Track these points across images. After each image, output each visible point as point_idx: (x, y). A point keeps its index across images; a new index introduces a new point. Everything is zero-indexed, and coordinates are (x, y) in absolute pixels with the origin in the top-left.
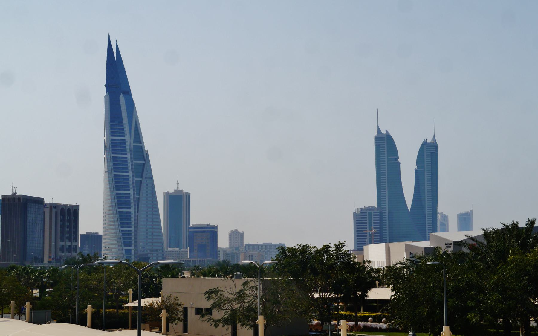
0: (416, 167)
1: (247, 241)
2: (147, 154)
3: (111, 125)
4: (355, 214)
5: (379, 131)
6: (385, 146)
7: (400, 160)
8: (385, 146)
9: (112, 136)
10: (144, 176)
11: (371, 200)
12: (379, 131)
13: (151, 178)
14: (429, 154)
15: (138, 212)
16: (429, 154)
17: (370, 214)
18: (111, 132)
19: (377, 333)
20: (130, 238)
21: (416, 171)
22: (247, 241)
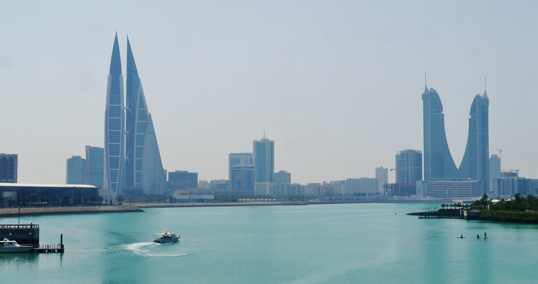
0: (470, 117)
1: (293, 181)
2: (150, 116)
3: (111, 96)
4: (397, 156)
5: (426, 89)
6: (432, 103)
7: (345, 179)
8: (432, 103)
9: (111, 104)
10: (147, 132)
11: (417, 143)
12: (426, 89)
13: (153, 133)
14: (480, 109)
15: (364, 195)
16: (480, 109)
17: (407, 155)
18: (111, 101)
19: (121, 85)
20: (117, 176)
21: (470, 120)
22: (293, 181)
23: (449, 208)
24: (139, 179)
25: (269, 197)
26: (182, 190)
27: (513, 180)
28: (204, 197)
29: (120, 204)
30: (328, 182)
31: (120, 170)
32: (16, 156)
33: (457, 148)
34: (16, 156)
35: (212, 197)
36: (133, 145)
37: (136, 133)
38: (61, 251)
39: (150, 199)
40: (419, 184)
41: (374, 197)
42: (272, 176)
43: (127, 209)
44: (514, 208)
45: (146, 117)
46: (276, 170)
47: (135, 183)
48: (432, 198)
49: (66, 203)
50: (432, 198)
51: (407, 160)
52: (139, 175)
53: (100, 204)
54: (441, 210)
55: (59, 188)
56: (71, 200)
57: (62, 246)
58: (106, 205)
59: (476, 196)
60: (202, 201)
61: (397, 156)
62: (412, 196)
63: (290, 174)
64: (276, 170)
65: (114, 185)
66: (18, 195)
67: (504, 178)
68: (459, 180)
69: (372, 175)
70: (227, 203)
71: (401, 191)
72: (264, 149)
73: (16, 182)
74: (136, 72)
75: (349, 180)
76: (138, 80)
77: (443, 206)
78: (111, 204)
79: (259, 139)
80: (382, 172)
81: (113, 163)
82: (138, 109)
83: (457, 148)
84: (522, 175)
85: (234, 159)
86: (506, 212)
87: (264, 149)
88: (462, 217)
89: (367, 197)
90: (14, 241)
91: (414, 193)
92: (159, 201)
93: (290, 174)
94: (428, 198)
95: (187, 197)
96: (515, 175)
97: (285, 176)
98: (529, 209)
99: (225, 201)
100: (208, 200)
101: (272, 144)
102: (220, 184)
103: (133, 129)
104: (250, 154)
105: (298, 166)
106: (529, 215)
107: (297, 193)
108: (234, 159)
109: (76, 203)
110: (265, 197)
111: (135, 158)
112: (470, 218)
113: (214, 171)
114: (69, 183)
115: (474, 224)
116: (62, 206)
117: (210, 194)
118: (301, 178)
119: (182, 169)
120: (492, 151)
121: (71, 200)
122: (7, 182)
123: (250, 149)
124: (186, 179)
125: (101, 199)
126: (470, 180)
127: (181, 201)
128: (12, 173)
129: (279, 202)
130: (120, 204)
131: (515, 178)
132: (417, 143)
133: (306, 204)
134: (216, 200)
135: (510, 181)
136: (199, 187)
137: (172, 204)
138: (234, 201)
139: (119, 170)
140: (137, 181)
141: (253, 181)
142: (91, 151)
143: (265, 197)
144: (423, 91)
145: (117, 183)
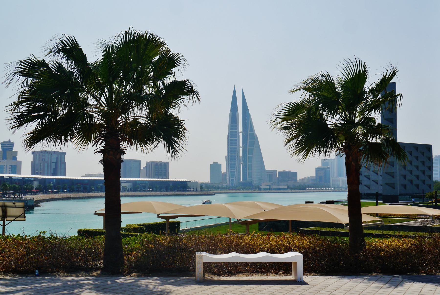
2: (257, 136)
13: (259, 147)
35: (286, 187)
37: (248, 148)
47: (248, 179)
49: (85, 190)
53: (188, 191)
55: (75, 179)
59: (122, 284)
60: (280, 189)
65: (232, 180)
78: (196, 190)
92: (71, 191)
99: (295, 189)
100: (284, 189)
114: (32, 174)
119: (287, 169)
122: (162, 178)
139: (235, 170)
145: (234, 178)
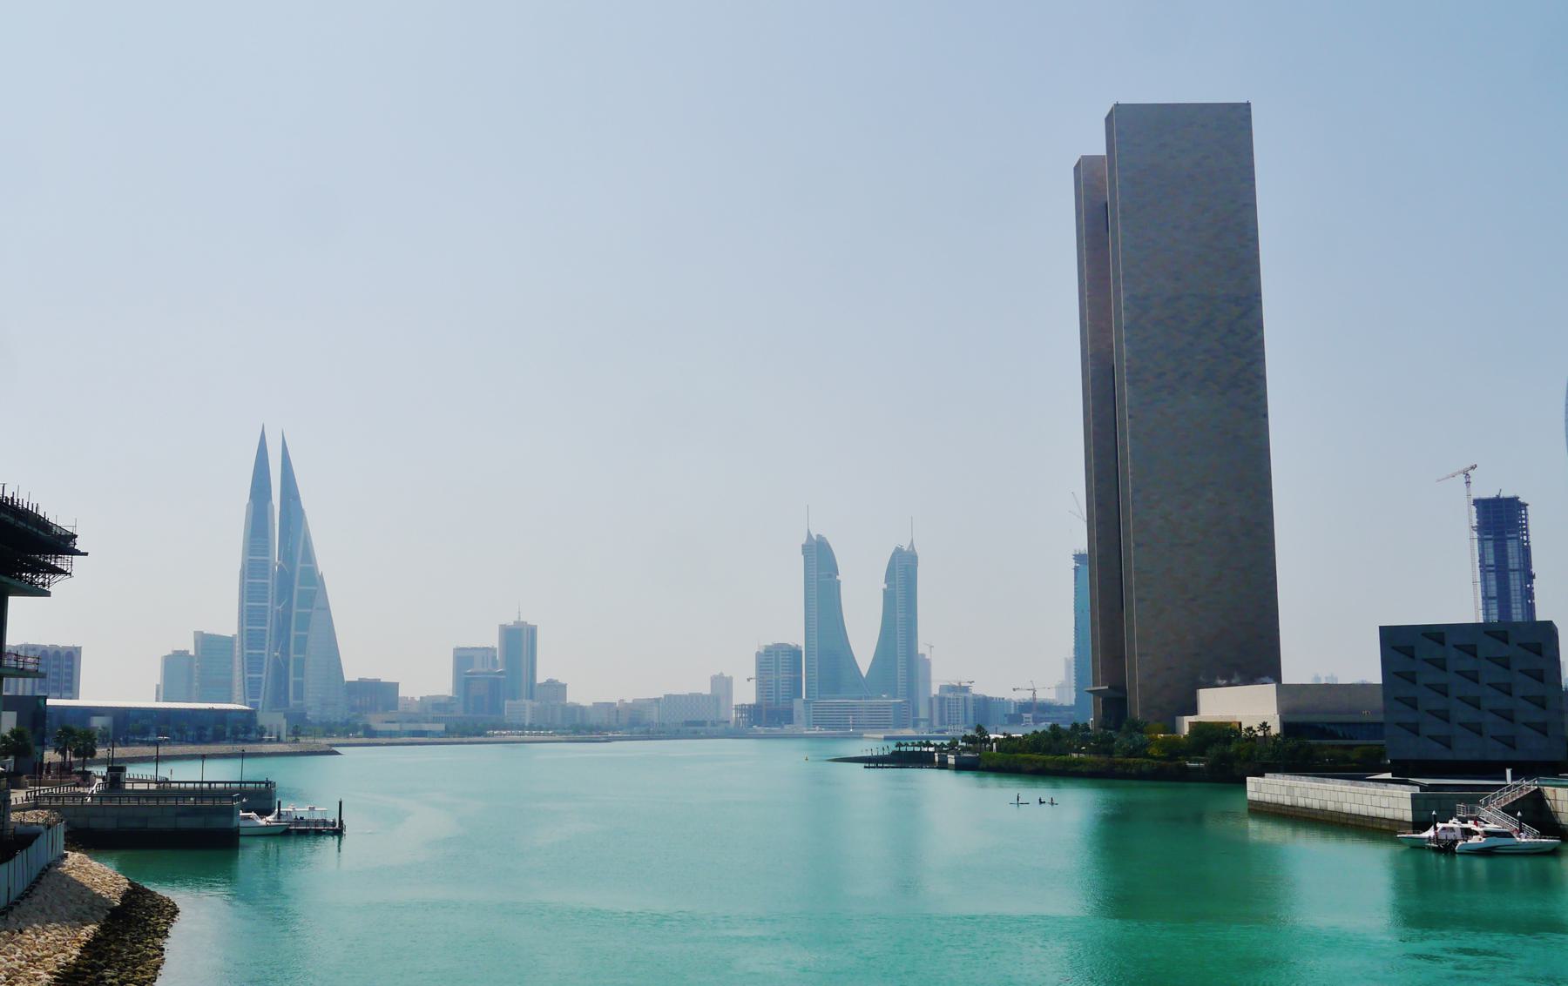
2: (321, 577)
5: (809, 536)
6: (820, 563)
8: (820, 563)
11: (794, 634)
12: (809, 536)
13: (327, 609)
14: (902, 574)
15: (703, 723)
16: (902, 574)
23: (910, 749)
24: (299, 694)
25: (531, 727)
26: (369, 716)
27: (965, 699)
28: (426, 727)
29: (296, 741)
30: (629, 701)
31: (265, 676)
32: (78, 650)
33: (864, 646)
34: (78, 650)
36: (289, 629)
37: (295, 610)
38: (338, 832)
39: (329, 729)
40: (798, 705)
41: (721, 727)
42: (532, 690)
43: (310, 748)
44: (1047, 751)
45: (314, 581)
46: (541, 678)
48: (824, 731)
50: (824, 731)
51: (775, 661)
52: (299, 687)
53: (261, 741)
54: (894, 753)
56: (209, 732)
57: (341, 822)
58: (270, 741)
60: (423, 734)
61: (758, 655)
62: (787, 727)
63: (565, 686)
64: (541, 678)
66: (115, 721)
67: (950, 695)
68: (867, 698)
69: (706, 690)
70: (466, 739)
71: (768, 717)
72: (519, 640)
73: (74, 694)
74: (297, 498)
75: (669, 697)
76: (301, 513)
77: (899, 745)
78: (279, 740)
79: (510, 621)
80: (722, 684)
81: (253, 664)
82: (299, 565)
83: (864, 646)
84: (978, 690)
85: (463, 659)
86: (1035, 756)
87: (519, 640)
88: (943, 765)
89: (709, 727)
90: (253, 814)
91: (790, 721)
93: (565, 686)
94: (817, 730)
95: (395, 727)
96: (966, 689)
97: (556, 688)
98: (1079, 751)
101: (533, 631)
102: (436, 706)
103: (290, 601)
104: (493, 650)
105: (581, 671)
106: (1080, 762)
107: (578, 721)
108: (463, 659)
109: (218, 738)
110: (522, 727)
111: (292, 656)
112: (961, 767)
113: (426, 679)
115: (967, 778)
116: (193, 743)
117: (436, 720)
118: (583, 693)
119: (370, 675)
120: (922, 649)
121: (209, 732)
123: (492, 640)
124: (380, 694)
125: (262, 731)
126: (885, 699)
127: (391, 734)
128: (71, 681)
129: (557, 737)
130: (296, 741)
131: (969, 696)
132: (794, 634)
133: (608, 740)
134: (448, 732)
135: (961, 702)
136: (400, 708)
137: (365, 740)
138: (479, 735)
139: (263, 676)
140: (296, 698)
141: (497, 701)
142: (206, 642)
143: (522, 727)
144: (804, 540)
